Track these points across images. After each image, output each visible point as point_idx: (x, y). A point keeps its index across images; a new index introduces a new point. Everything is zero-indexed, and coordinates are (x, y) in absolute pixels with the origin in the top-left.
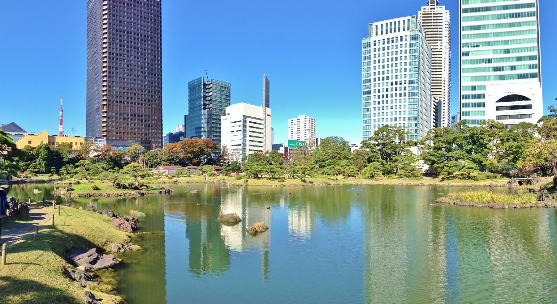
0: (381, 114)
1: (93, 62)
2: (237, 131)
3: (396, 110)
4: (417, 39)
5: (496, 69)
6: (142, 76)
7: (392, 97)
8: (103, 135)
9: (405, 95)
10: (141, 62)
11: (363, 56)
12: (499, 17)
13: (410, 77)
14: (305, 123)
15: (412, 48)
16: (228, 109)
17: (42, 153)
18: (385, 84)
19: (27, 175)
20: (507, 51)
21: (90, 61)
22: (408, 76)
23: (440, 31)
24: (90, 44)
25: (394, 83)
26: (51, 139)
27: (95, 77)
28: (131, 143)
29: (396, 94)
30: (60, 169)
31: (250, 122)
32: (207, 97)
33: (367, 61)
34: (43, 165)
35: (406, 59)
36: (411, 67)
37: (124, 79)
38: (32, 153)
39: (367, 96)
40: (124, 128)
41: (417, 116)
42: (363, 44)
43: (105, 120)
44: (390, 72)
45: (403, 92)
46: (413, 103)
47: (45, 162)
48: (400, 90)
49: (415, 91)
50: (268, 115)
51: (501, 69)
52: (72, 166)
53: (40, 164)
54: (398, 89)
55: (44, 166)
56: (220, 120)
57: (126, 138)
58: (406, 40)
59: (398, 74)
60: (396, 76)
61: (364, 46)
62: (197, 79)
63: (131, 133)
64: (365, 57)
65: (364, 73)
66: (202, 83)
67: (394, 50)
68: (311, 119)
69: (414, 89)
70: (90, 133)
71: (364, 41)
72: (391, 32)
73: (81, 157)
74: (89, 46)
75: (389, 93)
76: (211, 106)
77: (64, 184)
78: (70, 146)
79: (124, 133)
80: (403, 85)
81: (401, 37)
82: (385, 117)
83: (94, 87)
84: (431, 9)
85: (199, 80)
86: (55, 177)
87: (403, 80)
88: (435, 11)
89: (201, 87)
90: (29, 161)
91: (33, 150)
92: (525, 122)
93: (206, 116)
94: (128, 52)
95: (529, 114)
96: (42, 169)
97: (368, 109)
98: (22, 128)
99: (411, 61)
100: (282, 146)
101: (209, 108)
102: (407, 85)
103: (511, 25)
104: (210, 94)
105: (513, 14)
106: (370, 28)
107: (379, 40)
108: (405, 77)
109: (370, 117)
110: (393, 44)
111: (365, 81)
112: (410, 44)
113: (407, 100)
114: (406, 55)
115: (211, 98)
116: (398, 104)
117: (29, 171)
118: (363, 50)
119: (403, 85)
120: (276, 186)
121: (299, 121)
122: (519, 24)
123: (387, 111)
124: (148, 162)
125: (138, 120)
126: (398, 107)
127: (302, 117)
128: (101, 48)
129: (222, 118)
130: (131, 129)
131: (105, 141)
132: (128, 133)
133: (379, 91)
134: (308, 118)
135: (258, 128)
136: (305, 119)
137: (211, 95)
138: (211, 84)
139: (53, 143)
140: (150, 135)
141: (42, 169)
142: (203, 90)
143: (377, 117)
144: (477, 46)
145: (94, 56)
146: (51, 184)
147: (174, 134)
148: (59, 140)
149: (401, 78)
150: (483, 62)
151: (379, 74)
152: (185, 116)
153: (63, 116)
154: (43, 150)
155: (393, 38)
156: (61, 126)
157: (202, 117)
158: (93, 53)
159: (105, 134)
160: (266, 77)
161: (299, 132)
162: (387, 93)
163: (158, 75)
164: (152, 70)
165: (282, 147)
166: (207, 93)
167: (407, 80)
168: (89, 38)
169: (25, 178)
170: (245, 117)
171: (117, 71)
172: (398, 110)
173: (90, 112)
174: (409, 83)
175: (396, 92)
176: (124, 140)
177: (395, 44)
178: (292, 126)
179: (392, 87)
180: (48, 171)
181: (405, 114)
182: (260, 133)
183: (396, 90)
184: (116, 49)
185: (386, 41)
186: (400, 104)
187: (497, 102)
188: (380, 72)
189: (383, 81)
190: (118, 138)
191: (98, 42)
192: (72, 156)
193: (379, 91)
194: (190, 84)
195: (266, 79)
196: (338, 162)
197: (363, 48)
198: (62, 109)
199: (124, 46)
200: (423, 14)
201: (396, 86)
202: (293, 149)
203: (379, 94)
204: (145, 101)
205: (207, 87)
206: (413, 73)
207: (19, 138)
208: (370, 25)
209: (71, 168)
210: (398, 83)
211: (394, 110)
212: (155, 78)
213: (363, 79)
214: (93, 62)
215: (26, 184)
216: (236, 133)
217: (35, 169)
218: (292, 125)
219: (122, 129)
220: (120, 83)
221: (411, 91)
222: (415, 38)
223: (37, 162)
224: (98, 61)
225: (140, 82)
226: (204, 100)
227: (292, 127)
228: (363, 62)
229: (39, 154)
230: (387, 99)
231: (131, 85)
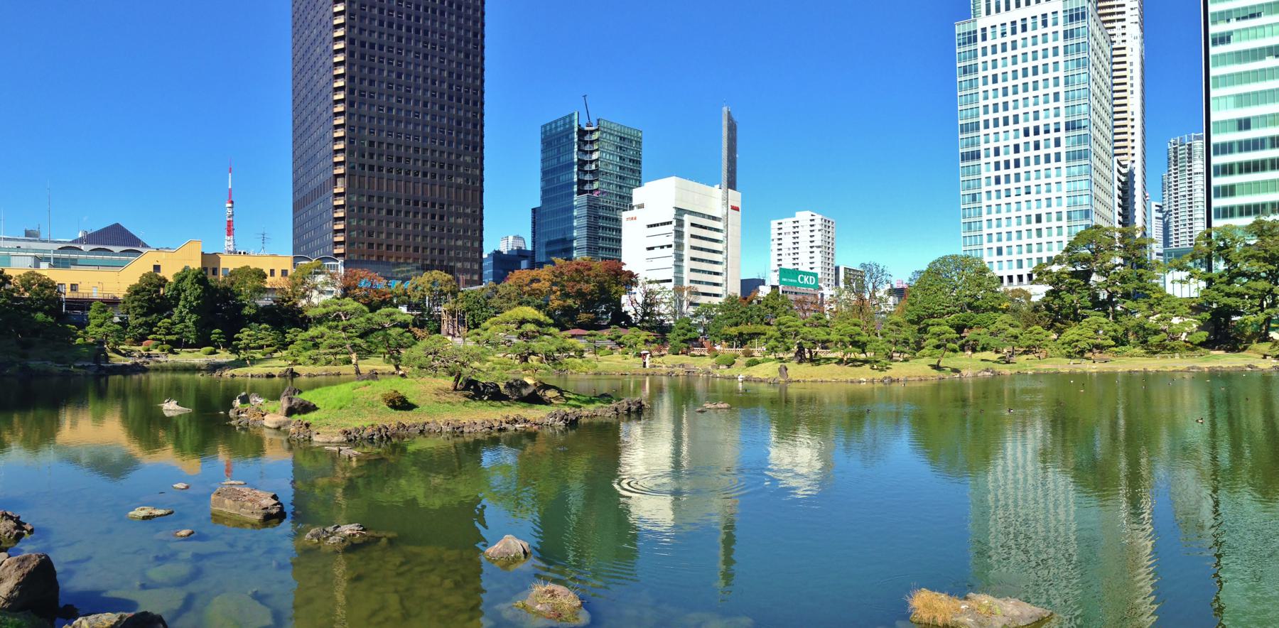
0: (1004, 208)
1: (308, 66)
2: (662, 247)
3: (1038, 197)
4: (1083, 17)
6: (434, 104)
7: (999, 169)
8: (336, 251)
9: (1058, 159)
10: (433, 68)
11: (958, 65)
13: (1067, 113)
14: (811, 231)
15: (1069, 43)
16: (638, 195)
17: (188, 292)
18: (1012, 134)
19: (148, 350)
21: (300, 66)
22: (1062, 111)
23: (1118, 13)
24: (300, 22)
25: (1031, 132)
26: (210, 260)
27: (313, 104)
28: (408, 271)
29: (1037, 157)
30: (236, 336)
31: (693, 225)
33: (968, 78)
34: (191, 324)
35: (1056, 69)
36: (1070, 88)
37: (390, 109)
38: (162, 292)
39: (971, 163)
40: (389, 235)
41: (1089, 207)
42: (959, 35)
43: (340, 214)
44: (1021, 103)
45: (1052, 150)
46: (1078, 178)
47: (194, 317)
48: (1047, 147)
49: (1083, 147)
50: (733, 208)
52: (268, 326)
53: (182, 321)
54: (1042, 145)
55: (193, 328)
56: (618, 221)
57: (393, 260)
58: (1055, 24)
59: (1041, 107)
60: (1036, 112)
61: (961, 41)
62: (564, 119)
63: (407, 247)
64: (965, 67)
65: (964, 107)
66: (576, 129)
67: (1030, 49)
68: (825, 221)
69: (1079, 142)
70: (303, 249)
71: (960, 28)
73: (290, 303)
74: (298, 25)
75: (1021, 155)
76: (596, 185)
77: (252, 376)
78: (261, 275)
79: (389, 247)
80: (1052, 135)
81: (1045, 15)
82: (1013, 214)
83: (312, 131)
85: (568, 120)
86: (224, 356)
87: (1052, 121)
89: (573, 138)
90: (155, 315)
91: (163, 286)
93: (585, 211)
94: (399, 39)
96: (188, 334)
97: (974, 195)
98: (139, 236)
99: (1069, 73)
100: (763, 282)
101: (591, 192)
102: (1062, 134)
104: (595, 156)
107: (994, 27)
108: (1057, 115)
109: (980, 214)
110: (1024, 35)
111: (965, 129)
112: (1065, 32)
113: (1064, 171)
114: (1056, 59)
115: (597, 166)
116: (1043, 181)
117: (153, 339)
118: (958, 51)
119: (1052, 135)
120: (872, 381)
121: (796, 224)
123: (1018, 199)
124: (466, 316)
125: (425, 215)
126: (1044, 188)
127: (803, 216)
128: (330, 26)
129: (625, 215)
130: (407, 237)
131: (343, 268)
132: (398, 247)
133: (997, 152)
134: (818, 218)
136: (811, 220)
137: (597, 160)
138: (597, 130)
139: (215, 271)
140: (452, 253)
141: (188, 334)
142: (576, 146)
143: (994, 216)
144: (1253, 16)
145: (311, 51)
146: (215, 375)
147: (505, 252)
148: (229, 263)
149: (1047, 117)
150: (1270, 54)
152: (534, 210)
153: (232, 215)
154: (189, 286)
155: (1024, 20)
156: (229, 238)
157: (575, 214)
158: (307, 44)
159: (340, 250)
160: (729, 113)
161: (796, 251)
162: (1017, 156)
163: (475, 104)
164: (460, 90)
165: (764, 284)
166: (586, 152)
167: (1062, 120)
168: (296, 5)
169: (143, 359)
170: (680, 212)
171: (372, 88)
172: (1043, 196)
173: (301, 196)
174: (1067, 129)
175: (1037, 153)
176: (388, 263)
177: (1029, 33)
178: (780, 237)
179: (1027, 139)
180: (202, 341)
181: (1060, 205)
182: (714, 252)
183: (1037, 147)
184: (371, 32)
185: (1008, 28)
186: (1048, 181)
188: (997, 104)
189: (1006, 128)
190: (374, 258)
191: (321, 12)
192: (265, 301)
193: (997, 152)
194: (546, 131)
195: (730, 119)
196: (978, 319)
197: (959, 44)
198: (230, 196)
199: (390, 25)
201: (1037, 138)
202: (790, 290)
203: (997, 159)
204: (442, 167)
205: (587, 138)
206: (1076, 103)
207: (128, 261)
209: (263, 332)
210: (1042, 130)
211: (1033, 196)
212: (467, 111)
213: (960, 122)
214: (308, 66)
215: (147, 374)
216: (657, 252)
217: (169, 334)
218: (780, 234)
219: (384, 236)
220: (380, 119)
221: (1071, 149)
222: (1077, 15)
223: (175, 318)
224: (320, 62)
225: (428, 118)
226: (579, 170)
227: (780, 239)
228: (959, 80)
229: (179, 294)
230: (1017, 170)
231: (406, 126)
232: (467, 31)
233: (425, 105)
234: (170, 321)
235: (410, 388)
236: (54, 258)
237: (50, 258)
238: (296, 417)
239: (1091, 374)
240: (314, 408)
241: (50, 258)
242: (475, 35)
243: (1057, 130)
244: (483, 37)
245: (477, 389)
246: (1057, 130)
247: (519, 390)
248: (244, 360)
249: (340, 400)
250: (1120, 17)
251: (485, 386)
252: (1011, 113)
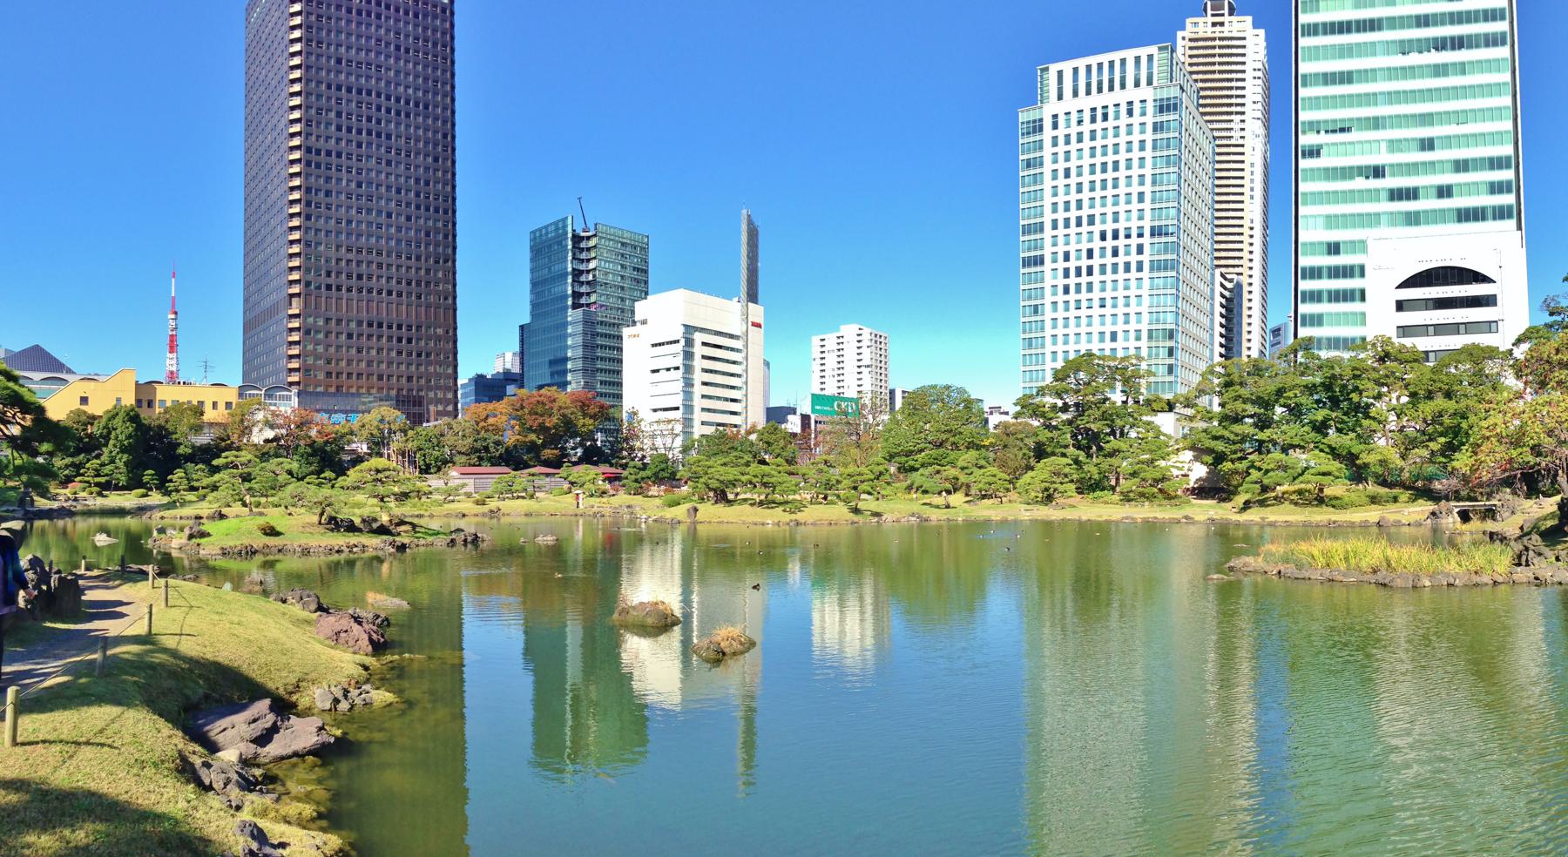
0: (1072, 322)
1: (262, 174)
2: (668, 369)
3: (1114, 311)
5: (1397, 195)
7: (1105, 273)
8: (290, 379)
9: (1140, 268)
10: (398, 176)
11: (1021, 157)
12: (1405, 48)
13: (1153, 216)
14: (859, 348)
15: (1159, 136)
16: (642, 309)
17: (118, 431)
18: (1085, 237)
19: (75, 493)
20: (1428, 144)
21: (253, 173)
22: (1148, 214)
23: (1237, 88)
24: (254, 125)
25: (1109, 235)
26: (145, 393)
27: (267, 217)
28: (370, 402)
29: (1115, 266)
30: (169, 477)
31: (704, 344)
32: (581, 272)
33: (1032, 172)
34: (121, 465)
35: (1142, 166)
36: (1157, 188)
37: (349, 222)
38: (89, 431)
39: (1033, 269)
40: (349, 362)
41: (1173, 327)
42: (1023, 123)
43: (295, 337)
44: (1098, 202)
45: (1134, 258)
46: (1162, 292)
47: (125, 457)
48: (1127, 253)
49: (1169, 257)
50: (754, 324)
51: (1411, 194)
52: (204, 467)
53: (112, 461)
54: (1121, 251)
55: (123, 469)
56: (620, 338)
57: (353, 390)
58: (1143, 114)
59: (1122, 208)
60: (1116, 214)
61: (1025, 131)
62: (556, 223)
63: (369, 375)
64: (1028, 160)
65: (1026, 206)
66: (570, 235)
67: (1110, 141)
68: (876, 335)
69: (1166, 251)
70: (254, 375)
71: (1024, 116)
73: (229, 442)
74: (251, 129)
75: (1096, 262)
76: (593, 298)
77: (181, 518)
78: (198, 410)
79: (349, 375)
80: (1134, 241)
81: (1130, 103)
82: (1083, 330)
83: (265, 245)
84: (1214, 24)
85: (560, 225)
86: (156, 498)
87: (1134, 224)
88: (1225, 31)
89: (567, 246)
90: (83, 455)
91: (92, 424)
92: (1478, 344)
93: (580, 328)
94: (359, 145)
95: (1490, 322)
96: (119, 476)
97: (1036, 306)
98: (63, 361)
99: (1158, 171)
100: (793, 411)
101: (588, 305)
102: (1146, 240)
103: (1440, 70)
104: (592, 265)
105: (1444, 39)
106: (1042, 78)
107: (1068, 114)
108: (1141, 218)
109: (1043, 329)
110: (1105, 125)
111: (1027, 230)
112: (1155, 124)
113: (1146, 283)
114: (1142, 154)
115: (594, 276)
116: (1121, 293)
117: (80, 482)
118: (1021, 141)
119: (1134, 241)
120: (778, 524)
121: (841, 340)
122: (1462, 68)
123: (1089, 312)
124: (418, 456)
125: (390, 338)
126: (1121, 301)
127: (849, 331)
128: (285, 134)
129: (626, 332)
130: (369, 363)
131: (296, 399)
132: (359, 375)
133: (1067, 257)
134: (866, 333)
135: (727, 361)
136: (859, 335)
137: (595, 269)
138: (595, 235)
139: (150, 404)
140: (423, 381)
141: (119, 476)
142: (570, 254)
143: (1060, 331)
144: (1342, 130)
145: (266, 157)
146: (144, 517)
147: (489, 377)
148: (167, 395)
149: (1128, 219)
150: (1360, 175)
151: (1067, 209)
152: (522, 327)
153: (176, 328)
154: (120, 424)
155: (1105, 107)
156: (171, 356)
157: (569, 331)
158: (261, 150)
159: (295, 378)
160: (749, 216)
161: (841, 371)
162: (1090, 262)
163: (446, 212)
164: (429, 198)
165: (795, 413)
166: (582, 261)
167: (1147, 224)
168: (250, 106)
169: (70, 503)
170: (689, 329)
171: (328, 200)
172: (1121, 310)
173: (253, 315)
174: (1152, 235)
175: (1115, 260)
176: (348, 394)
177: (1111, 123)
178: (823, 356)
179: (1103, 244)
180: (134, 483)
181: (1139, 321)
182: (732, 375)
183: (1115, 253)
184: (328, 138)
185: (1087, 116)
186: (1127, 293)
187: (1399, 287)
188: (1069, 202)
189: (1079, 230)
190: (332, 390)
191: (277, 117)
193: (1067, 257)
194: (535, 238)
195: (750, 222)
196: (952, 457)
197: (1023, 134)
198: (173, 307)
199: (349, 130)
200: (1190, 40)
201: (1115, 243)
202: (825, 419)
203: (1067, 265)
204: (409, 284)
205: (583, 245)
206: (1164, 205)
207: (54, 390)
208: (1042, 70)
209: (199, 473)
210: (1122, 234)
211: (1108, 311)
212: (436, 220)
213: (1022, 223)
214: (262, 174)
215: (74, 519)
216: (663, 375)
217: (98, 475)
218: (822, 352)
219: (344, 363)
220: (339, 233)
221: (1156, 258)
222: (1168, 106)
223: (105, 458)
224: (275, 172)
225: (393, 230)
226: (573, 281)
227: (822, 358)
228: (1021, 174)
229: (109, 433)
230: (1090, 279)
231: (367, 240)
232: (436, 132)
233: (389, 215)
234: (99, 462)
235: (275, 517)
238: (194, 540)
240: (209, 535)
242: (445, 136)
244: (453, 137)
245: (336, 523)
247: (370, 524)
248: (174, 502)
249: (228, 529)
251: (342, 521)
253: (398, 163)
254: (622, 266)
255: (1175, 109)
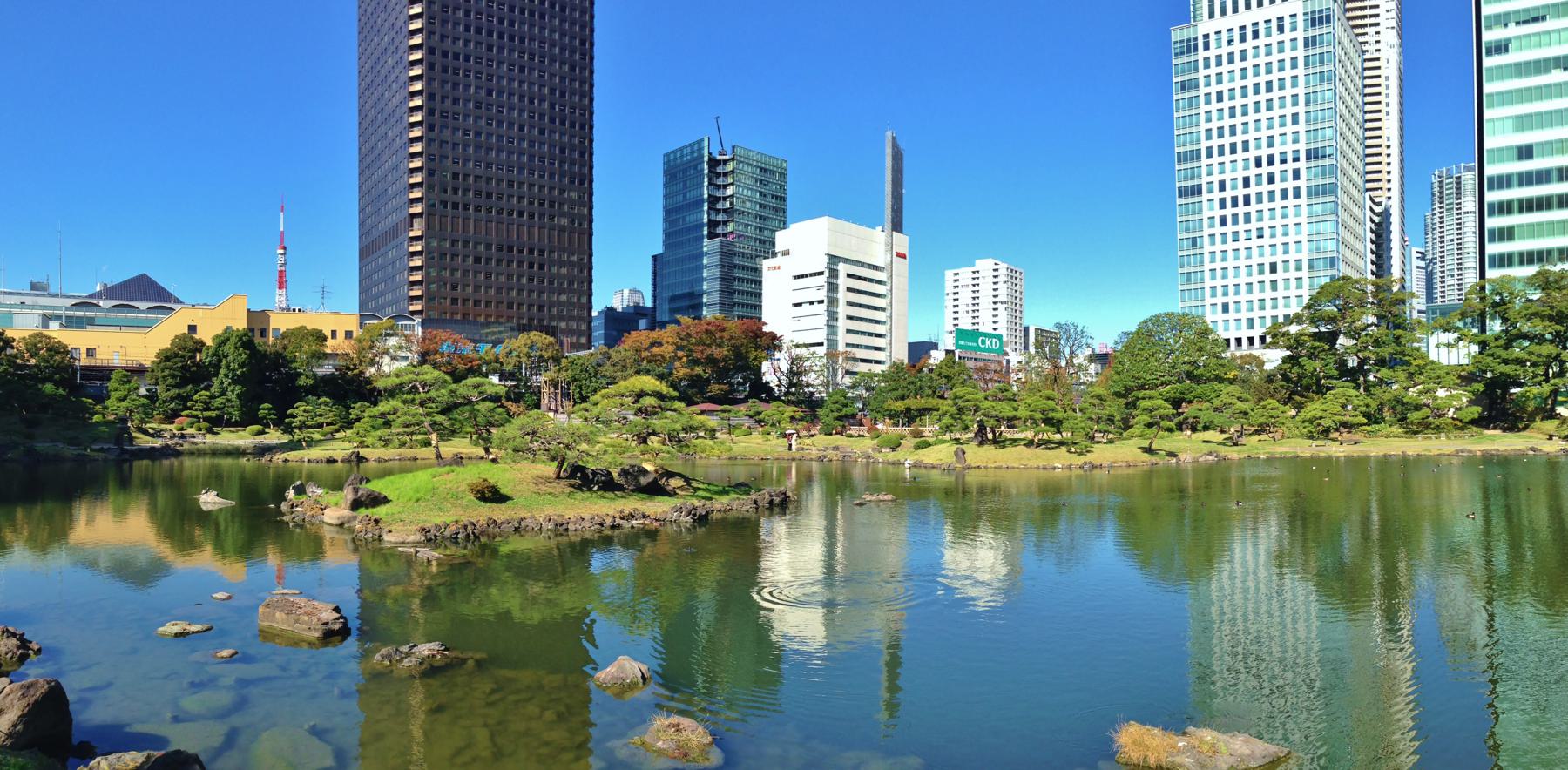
0: (1230, 255)
1: (378, 80)
2: (812, 303)
3: (1273, 241)
7: (1225, 208)
8: (412, 308)
9: (1297, 195)
10: (531, 84)
11: (1175, 80)
13: (1308, 139)
14: (995, 283)
15: (1310, 52)
16: (782, 239)
17: (230, 358)
18: (1240, 164)
19: (182, 429)
21: (368, 81)
22: (1303, 137)
23: (1371, 16)
24: (368, 27)
25: (1265, 161)
26: (257, 319)
27: (384, 128)
28: (500, 332)
29: (1271, 193)
30: (289, 412)
31: (849, 275)
32: (718, 199)
33: (1187, 95)
34: (234, 397)
35: (1294, 85)
36: (1311, 108)
37: (478, 134)
38: (198, 358)
39: (1190, 200)
40: (477, 288)
41: (1335, 254)
42: (1176, 42)
43: (417, 262)
44: (1251, 126)
45: (1290, 184)
46: (1321, 219)
47: (238, 389)
48: (1284, 180)
49: (1327, 181)
50: (899, 255)
52: (328, 400)
53: (223, 393)
54: (1277, 177)
55: (236, 402)
56: (758, 271)
57: (482, 319)
58: (1294, 29)
59: (1276, 131)
60: (1270, 138)
61: (1179, 51)
62: (691, 145)
63: (499, 303)
64: (1183, 82)
65: (1181, 132)
66: (706, 159)
67: (1262, 60)
68: (1012, 271)
69: (1323, 174)
70: (372, 305)
71: (1177, 35)
72: (1223, 12)
73: (356, 372)
74: (365, 31)
75: (1252, 191)
76: (730, 227)
77: (309, 461)
78: (320, 337)
79: (477, 303)
80: (1290, 166)
81: (1281, 19)
82: (1242, 262)
83: (383, 160)
85: (696, 147)
86: (274, 437)
87: (1289, 148)
89: (703, 170)
90: (190, 386)
91: (200, 351)
93: (717, 259)
94: (490, 48)
96: (231, 410)
97: (1194, 239)
98: (170, 289)
99: (1311, 90)
100: (935, 346)
101: (725, 235)
102: (1302, 164)
104: (729, 191)
107: (1218, 33)
108: (1296, 141)
109: (1202, 263)
110: (1256, 43)
111: (1183, 158)
112: (1306, 39)
113: (1304, 210)
114: (1294, 72)
115: (731, 203)
116: (1279, 222)
117: (188, 416)
118: (1174, 62)
119: (1290, 166)
121: (976, 275)
123: (1248, 244)
124: (572, 388)
125: (520, 264)
126: (1279, 230)
127: (985, 265)
128: (405, 32)
129: (766, 264)
130: (499, 290)
131: (420, 328)
132: (488, 303)
133: (1222, 186)
134: (1003, 267)
136: (995, 270)
137: (732, 196)
138: (732, 159)
139: (263, 333)
140: (554, 311)
141: (231, 410)
142: (706, 179)
143: (1218, 265)
144: (1536, 19)
145: (382, 62)
146: (263, 460)
147: (619, 310)
148: (281, 322)
149: (1283, 143)
150: (1557, 66)
152: (655, 258)
153: (285, 264)
154: (232, 350)
155: (1255, 24)
156: (280, 292)
157: (705, 262)
158: (377, 54)
159: (417, 307)
160: (894, 138)
161: (976, 307)
162: (1247, 191)
163: (582, 127)
164: (564, 110)
165: (936, 348)
166: (718, 187)
167: (1302, 147)
168: (363, 6)
169: (176, 440)
170: (834, 259)
171: (456, 108)
172: (1279, 240)
173: (369, 240)
174: (1308, 158)
175: (1271, 187)
176: (475, 322)
177: (1262, 41)
178: (956, 290)
179: (1259, 171)
180: (248, 418)
181: (1299, 251)
182: (876, 308)
183: (1271, 180)
184: (455, 39)
185: (1236, 35)
186: (1285, 221)
188: (1222, 128)
189: (1234, 157)
190: (459, 317)
191: (394, 15)
193: (1222, 186)
194: (669, 161)
195: (895, 145)
196: (1199, 391)
197: (1176, 54)
198: (282, 240)
199: (478, 31)
201: (1271, 169)
202: (969, 355)
203: (1222, 195)
204: (542, 204)
205: (720, 169)
206: (1319, 126)
207: (157, 320)
209: (323, 407)
210: (1277, 159)
211: (1266, 241)
212: (572, 136)
213: (1177, 150)
214: (378, 80)
215: (180, 458)
216: (806, 309)
217: (207, 409)
218: (956, 287)
219: (470, 289)
220: (466, 146)
221: (1313, 183)
222: (1321, 18)
223: (215, 389)
224: (393, 76)
225: (525, 145)
226: (709, 208)
227: (956, 293)
228: (1175, 98)
229: (220, 361)
230: (1247, 209)
231: (497, 155)
236: (66, 317)
237: (61, 317)
239: (1337, 458)
241: (61, 317)
243: (1296, 160)
246: (1296, 160)
250: (1373, 20)
252: (1239, 139)
253: (531, 69)
254: (761, 193)
255: (1328, 21)
